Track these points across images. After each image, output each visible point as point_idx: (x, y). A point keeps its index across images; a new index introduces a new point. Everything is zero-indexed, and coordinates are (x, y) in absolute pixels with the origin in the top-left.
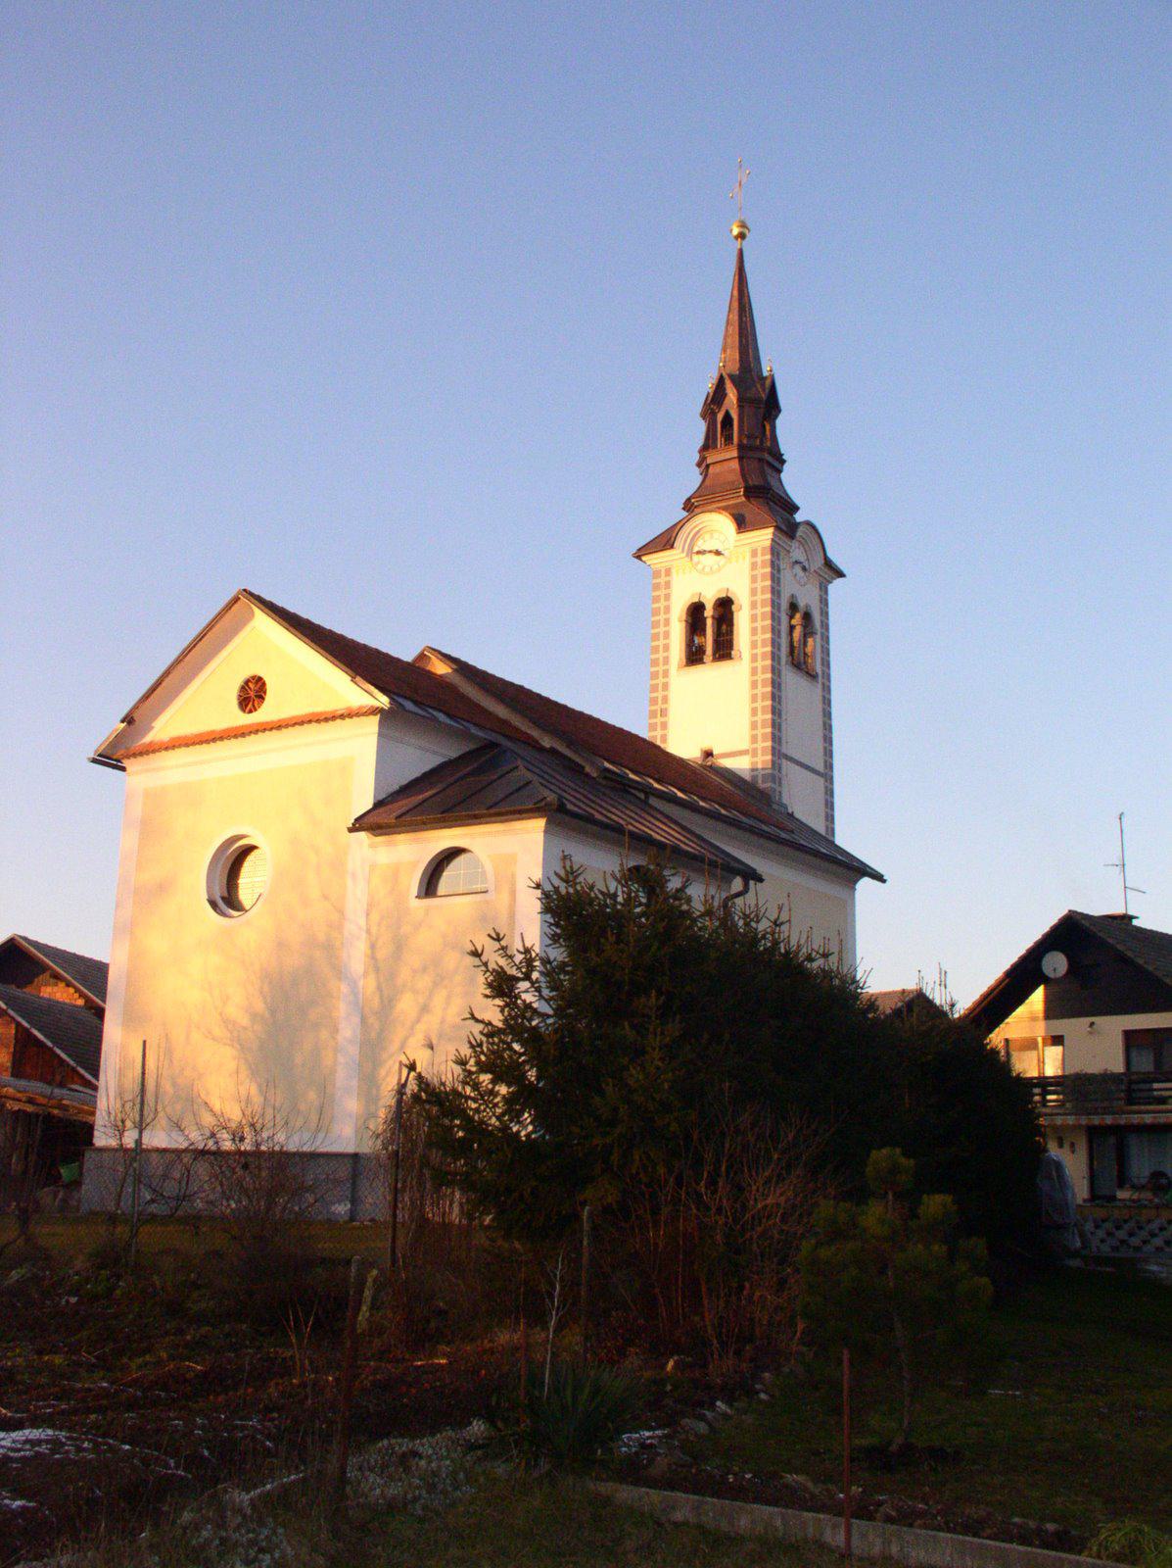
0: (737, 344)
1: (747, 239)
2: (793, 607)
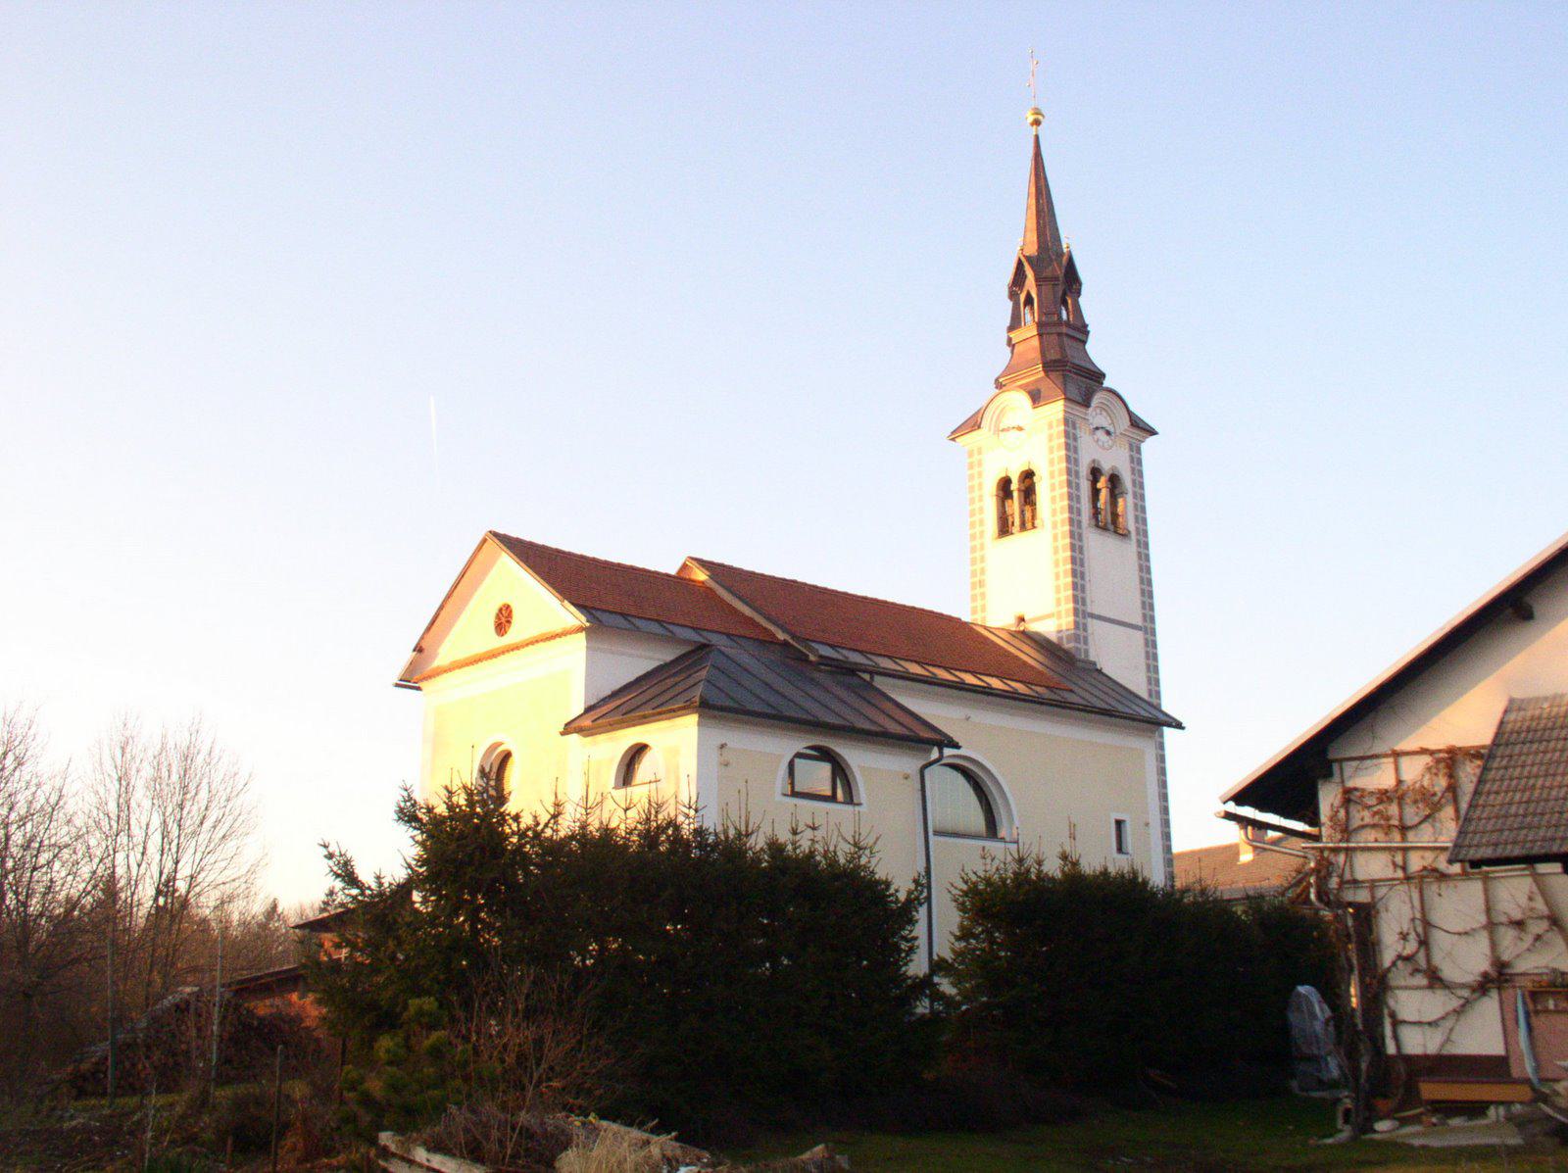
0: (1035, 226)
1: (1043, 124)
2: (1095, 473)
